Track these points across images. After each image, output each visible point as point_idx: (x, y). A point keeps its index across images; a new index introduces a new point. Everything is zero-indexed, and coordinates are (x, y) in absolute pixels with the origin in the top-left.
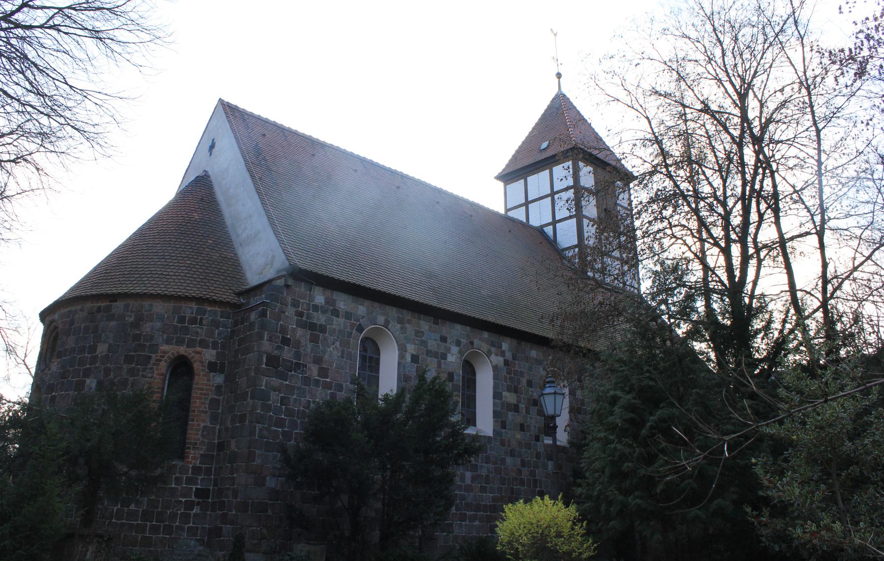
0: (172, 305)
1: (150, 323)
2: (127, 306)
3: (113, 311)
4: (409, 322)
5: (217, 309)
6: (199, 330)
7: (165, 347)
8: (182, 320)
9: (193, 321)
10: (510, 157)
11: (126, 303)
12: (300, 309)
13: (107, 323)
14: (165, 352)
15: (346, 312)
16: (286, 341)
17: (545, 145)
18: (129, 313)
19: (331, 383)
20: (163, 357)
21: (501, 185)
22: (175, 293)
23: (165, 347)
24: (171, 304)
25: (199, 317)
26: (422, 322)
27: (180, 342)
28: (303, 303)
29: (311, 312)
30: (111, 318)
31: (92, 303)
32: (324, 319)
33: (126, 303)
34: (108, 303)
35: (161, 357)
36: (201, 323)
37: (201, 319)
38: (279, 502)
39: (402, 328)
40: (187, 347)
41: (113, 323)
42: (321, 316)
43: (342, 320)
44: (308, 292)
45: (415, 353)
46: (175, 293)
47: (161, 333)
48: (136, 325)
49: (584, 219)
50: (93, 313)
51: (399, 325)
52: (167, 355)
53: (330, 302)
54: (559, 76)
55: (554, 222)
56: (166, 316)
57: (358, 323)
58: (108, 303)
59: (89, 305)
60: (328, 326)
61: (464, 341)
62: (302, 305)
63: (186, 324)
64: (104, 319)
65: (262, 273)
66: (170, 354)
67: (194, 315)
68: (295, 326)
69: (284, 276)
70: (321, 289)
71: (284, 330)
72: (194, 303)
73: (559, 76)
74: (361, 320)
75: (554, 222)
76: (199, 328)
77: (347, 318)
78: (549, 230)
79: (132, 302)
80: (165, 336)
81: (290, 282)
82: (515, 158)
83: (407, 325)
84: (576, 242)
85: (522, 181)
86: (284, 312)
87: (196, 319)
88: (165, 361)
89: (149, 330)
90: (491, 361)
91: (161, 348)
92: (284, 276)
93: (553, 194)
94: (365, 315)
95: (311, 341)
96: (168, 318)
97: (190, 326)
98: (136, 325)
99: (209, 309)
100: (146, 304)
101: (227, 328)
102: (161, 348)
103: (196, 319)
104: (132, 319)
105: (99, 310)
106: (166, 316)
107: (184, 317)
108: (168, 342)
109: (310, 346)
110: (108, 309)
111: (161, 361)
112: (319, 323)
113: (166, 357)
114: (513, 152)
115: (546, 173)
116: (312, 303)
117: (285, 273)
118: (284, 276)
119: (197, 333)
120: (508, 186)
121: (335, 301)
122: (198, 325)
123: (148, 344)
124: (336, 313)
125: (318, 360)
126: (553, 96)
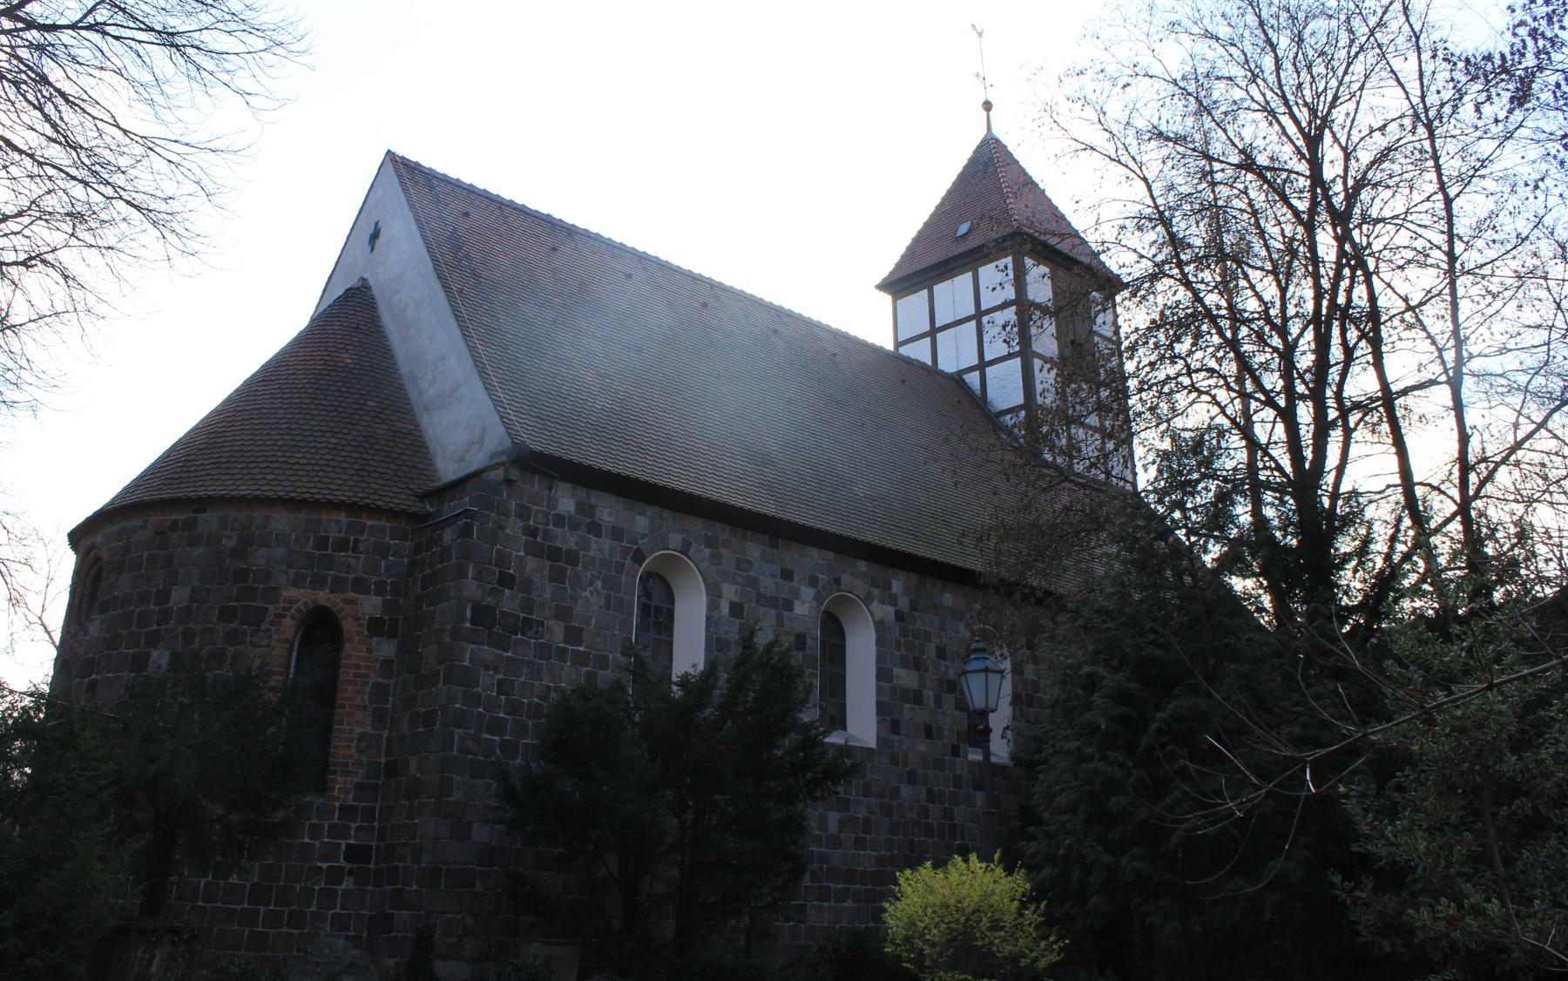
0: (303, 516)
5: (383, 523)
6: (353, 562)
7: (291, 593)
8: (322, 543)
9: (342, 545)
10: (903, 250)
13: (189, 549)
14: (292, 602)
16: (506, 580)
18: (228, 532)
19: (587, 654)
20: (288, 609)
21: (887, 299)
23: (291, 593)
25: (352, 538)
27: (318, 583)
29: (551, 527)
32: (574, 540)
35: (284, 609)
36: (355, 549)
37: (356, 541)
38: (496, 868)
39: (713, 556)
40: (332, 591)
42: (568, 535)
43: (606, 542)
44: (547, 492)
45: (736, 599)
47: (284, 567)
51: (707, 550)
52: (295, 607)
53: (585, 509)
54: (988, 106)
55: (982, 366)
56: (293, 536)
57: (635, 547)
59: (155, 519)
60: (582, 553)
61: (823, 578)
63: (329, 552)
65: (463, 460)
66: (300, 604)
67: (342, 535)
68: (522, 553)
70: (569, 486)
71: (502, 560)
72: (343, 514)
73: (988, 106)
74: (640, 542)
75: (982, 366)
76: (353, 557)
78: (973, 379)
80: (292, 572)
82: (912, 252)
83: (723, 550)
86: (502, 528)
87: (346, 541)
88: (293, 617)
90: (872, 614)
91: (285, 594)
92: (503, 465)
95: (551, 580)
97: (336, 554)
99: (369, 523)
100: (259, 514)
101: (402, 557)
102: (285, 594)
103: (346, 541)
104: (232, 543)
105: (174, 526)
106: (293, 536)
107: (327, 538)
108: (297, 582)
109: (549, 587)
111: (285, 616)
112: (564, 547)
113: (292, 611)
117: (504, 458)
118: (503, 464)
119: (349, 566)
120: (899, 302)
121: (593, 507)
122: (350, 553)
124: (595, 529)
125: (563, 614)
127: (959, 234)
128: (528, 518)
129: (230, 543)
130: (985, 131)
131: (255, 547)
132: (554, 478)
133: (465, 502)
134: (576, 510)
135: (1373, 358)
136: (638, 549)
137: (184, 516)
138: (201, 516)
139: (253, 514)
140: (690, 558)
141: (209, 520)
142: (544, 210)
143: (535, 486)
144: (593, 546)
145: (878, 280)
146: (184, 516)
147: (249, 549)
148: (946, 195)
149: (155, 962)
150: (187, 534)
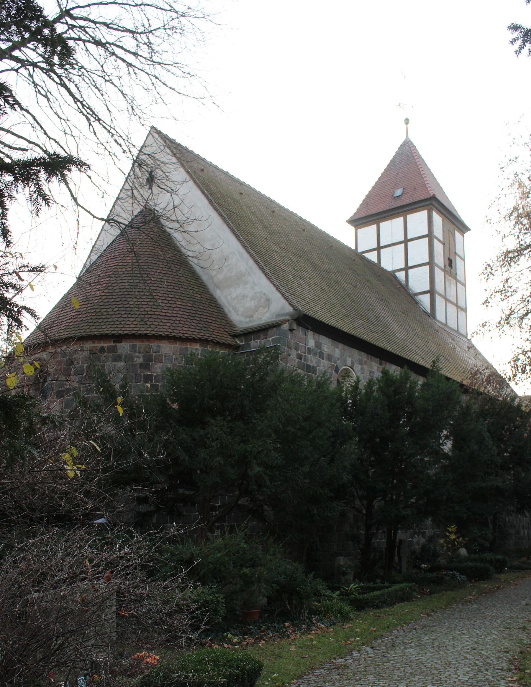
0: (178, 346)
1: (159, 364)
2: (134, 347)
3: (119, 352)
4: (366, 363)
10: (361, 202)
11: (132, 344)
12: (300, 352)
13: (114, 363)
15: (328, 355)
17: (398, 192)
18: (137, 354)
21: (352, 229)
22: (182, 335)
24: (178, 345)
26: (373, 363)
28: (302, 346)
29: (306, 354)
30: (118, 358)
31: (93, 343)
32: (315, 361)
33: (132, 344)
34: (112, 344)
41: (121, 364)
42: (313, 359)
44: (304, 336)
46: (149, 332)
48: (146, 365)
49: (436, 267)
50: (96, 353)
51: (360, 366)
53: (318, 345)
54: (407, 121)
55: (407, 269)
56: (174, 357)
57: (336, 365)
58: (112, 344)
59: (88, 345)
60: (318, 368)
62: (301, 348)
64: (110, 359)
69: (288, 321)
72: (199, 344)
73: (407, 121)
75: (407, 269)
77: (329, 360)
78: (401, 275)
79: (138, 344)
81: (295, 326)
82: (366, 203)
83: (365, 366)
84: (427, 288)
85: (375, 225)
86: (289, 355)
89: (159, 371)
92: (288, 321)
93: (406, 241)
94: (339, 357)
96: (176, 359)
98: (146, 365)
100: (154, 345)
104: (141, 360)
105: (102, 350)
106: (174, 357)
110: (113, 350)
114: (364, 197)
115: (401, 220)
116: (307, 347)
117: (288, 317)
120: (359, 231)
123: (160, 384)
124: (321, 355)
126: (401, 143)
127: (395, 195)
128: (298, 351)
129: (139, 360)
130: (406, 137)
131: (154, 362)
132: (308, 329)
133: (270, 340)
134: (315, 345)
135: (369, 262)
136: (337, 366)
137: (109, 344)
138: (119, 345)
139: (151, 344)
140: (354, 370)
141: (124, 347)
142: (225, 170)
143: (299, 332)
144: (322, 365)
145: (348, 218)
146: (109, 344)
147: (150, 364)
148: (384, 172)
149: (379, 592)
150: (111, 354)
